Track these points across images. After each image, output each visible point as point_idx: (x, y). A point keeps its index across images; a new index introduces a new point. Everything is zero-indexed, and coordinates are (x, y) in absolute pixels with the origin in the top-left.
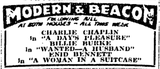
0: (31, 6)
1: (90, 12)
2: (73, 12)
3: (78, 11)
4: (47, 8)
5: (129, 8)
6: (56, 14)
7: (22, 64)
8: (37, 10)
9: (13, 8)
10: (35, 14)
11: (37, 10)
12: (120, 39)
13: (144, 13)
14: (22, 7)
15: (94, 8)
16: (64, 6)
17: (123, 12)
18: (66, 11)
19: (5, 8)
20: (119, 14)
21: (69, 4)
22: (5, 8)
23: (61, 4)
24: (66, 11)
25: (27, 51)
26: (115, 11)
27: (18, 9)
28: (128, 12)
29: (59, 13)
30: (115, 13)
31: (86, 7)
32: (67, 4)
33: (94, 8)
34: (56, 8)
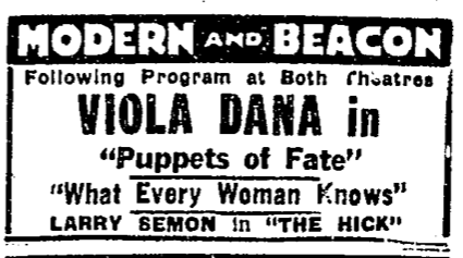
1: (277, 52)
3: (214, 39)
4: (127, 34)
5: (376, 30)
7: (245, 234)
8: (98, 39)
9: (33, 21)
11: (98, 39)
12: (398, 84)
13: (350, 44)
16: (420, 31)
17: (54, 35)
19: (14, 23)
20: (348, 51)
21: (188, 18)
22: (14, 23)
25: (404, 184)
26: (340, 40)
28: (374, 41)
30: (214, 42)
32: (180, 20)
34: (151, 35)
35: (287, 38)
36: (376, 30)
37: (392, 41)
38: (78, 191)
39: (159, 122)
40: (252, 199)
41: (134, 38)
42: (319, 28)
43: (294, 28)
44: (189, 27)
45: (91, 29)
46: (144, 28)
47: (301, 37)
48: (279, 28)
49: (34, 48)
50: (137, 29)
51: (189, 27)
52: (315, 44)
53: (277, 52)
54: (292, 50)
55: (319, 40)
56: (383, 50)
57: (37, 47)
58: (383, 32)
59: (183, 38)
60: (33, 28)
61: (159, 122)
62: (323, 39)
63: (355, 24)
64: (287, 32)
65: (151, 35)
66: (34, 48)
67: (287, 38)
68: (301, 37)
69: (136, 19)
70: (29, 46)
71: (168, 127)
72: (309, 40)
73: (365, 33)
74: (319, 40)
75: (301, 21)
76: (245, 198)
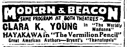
0: (24, 6)
1: (69, 13)
2: (57, 13)
5: (97, 8)
6: (43, 14)
9: (10, 7)
10: (27, 13)
14: (17, 7)
15: (71, 11)
17: (31, 11)
18: (51, 8)
19: (4, 7)
20: (89, 13)
22: (4, 7)
23: (46, 6)
24: (51, 8)
26: (86, 10)
27: (14, 9)
28: (95, 11)
29: (44, 13)
30: (86, 12)
31: (65, 7)
32: (51, 6)
33: (71, 11)
35: (71, 10)
36: (97, 8)
37: (22, 10)
38: (69, 27)
39: (11, 28)
40: (73, 25)
41: (37, 10)
42: (80, 8)
43: (73, 8)
44: (54, 7)
45: (27, 8)
46: (40, 8)
47: (75, 10)
48: (69, 8)
49: (10, 17)
50: (38, 8)
51: (54, 7)
52: (79, 11)
53: (69, 13)
54: (73, 12)
55: (80, 10)
56: (99, 12)
57: (12, 16)
58: (99, 8)
59: (53, 10)
60: (10, 9)
61: (11, 28)
62: (81, 10)
63: (90, 7)
64: (71, 8)
65: (42, 9)
66: (10, 17)
67: (71, 10)
68: (75, 10)
69: (39, 6)
70: (8, 16)
71: (13, 29)
72: (34, 10)
73: (93, 9)
74: (80, 10)
75: (75, 6)
76: (59, 27)
